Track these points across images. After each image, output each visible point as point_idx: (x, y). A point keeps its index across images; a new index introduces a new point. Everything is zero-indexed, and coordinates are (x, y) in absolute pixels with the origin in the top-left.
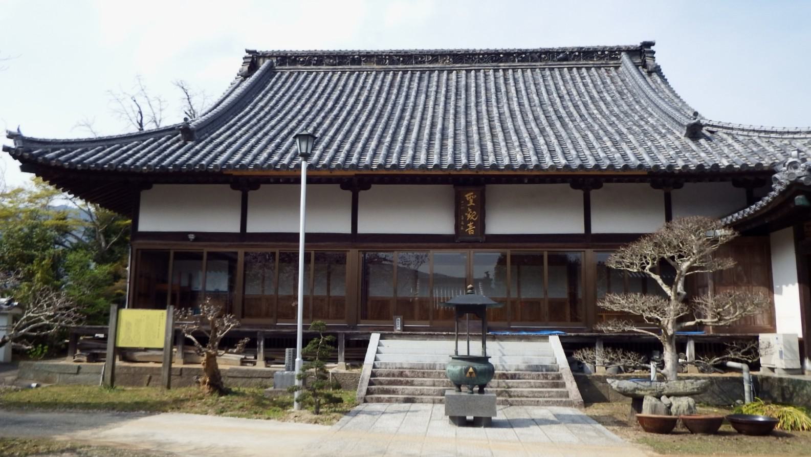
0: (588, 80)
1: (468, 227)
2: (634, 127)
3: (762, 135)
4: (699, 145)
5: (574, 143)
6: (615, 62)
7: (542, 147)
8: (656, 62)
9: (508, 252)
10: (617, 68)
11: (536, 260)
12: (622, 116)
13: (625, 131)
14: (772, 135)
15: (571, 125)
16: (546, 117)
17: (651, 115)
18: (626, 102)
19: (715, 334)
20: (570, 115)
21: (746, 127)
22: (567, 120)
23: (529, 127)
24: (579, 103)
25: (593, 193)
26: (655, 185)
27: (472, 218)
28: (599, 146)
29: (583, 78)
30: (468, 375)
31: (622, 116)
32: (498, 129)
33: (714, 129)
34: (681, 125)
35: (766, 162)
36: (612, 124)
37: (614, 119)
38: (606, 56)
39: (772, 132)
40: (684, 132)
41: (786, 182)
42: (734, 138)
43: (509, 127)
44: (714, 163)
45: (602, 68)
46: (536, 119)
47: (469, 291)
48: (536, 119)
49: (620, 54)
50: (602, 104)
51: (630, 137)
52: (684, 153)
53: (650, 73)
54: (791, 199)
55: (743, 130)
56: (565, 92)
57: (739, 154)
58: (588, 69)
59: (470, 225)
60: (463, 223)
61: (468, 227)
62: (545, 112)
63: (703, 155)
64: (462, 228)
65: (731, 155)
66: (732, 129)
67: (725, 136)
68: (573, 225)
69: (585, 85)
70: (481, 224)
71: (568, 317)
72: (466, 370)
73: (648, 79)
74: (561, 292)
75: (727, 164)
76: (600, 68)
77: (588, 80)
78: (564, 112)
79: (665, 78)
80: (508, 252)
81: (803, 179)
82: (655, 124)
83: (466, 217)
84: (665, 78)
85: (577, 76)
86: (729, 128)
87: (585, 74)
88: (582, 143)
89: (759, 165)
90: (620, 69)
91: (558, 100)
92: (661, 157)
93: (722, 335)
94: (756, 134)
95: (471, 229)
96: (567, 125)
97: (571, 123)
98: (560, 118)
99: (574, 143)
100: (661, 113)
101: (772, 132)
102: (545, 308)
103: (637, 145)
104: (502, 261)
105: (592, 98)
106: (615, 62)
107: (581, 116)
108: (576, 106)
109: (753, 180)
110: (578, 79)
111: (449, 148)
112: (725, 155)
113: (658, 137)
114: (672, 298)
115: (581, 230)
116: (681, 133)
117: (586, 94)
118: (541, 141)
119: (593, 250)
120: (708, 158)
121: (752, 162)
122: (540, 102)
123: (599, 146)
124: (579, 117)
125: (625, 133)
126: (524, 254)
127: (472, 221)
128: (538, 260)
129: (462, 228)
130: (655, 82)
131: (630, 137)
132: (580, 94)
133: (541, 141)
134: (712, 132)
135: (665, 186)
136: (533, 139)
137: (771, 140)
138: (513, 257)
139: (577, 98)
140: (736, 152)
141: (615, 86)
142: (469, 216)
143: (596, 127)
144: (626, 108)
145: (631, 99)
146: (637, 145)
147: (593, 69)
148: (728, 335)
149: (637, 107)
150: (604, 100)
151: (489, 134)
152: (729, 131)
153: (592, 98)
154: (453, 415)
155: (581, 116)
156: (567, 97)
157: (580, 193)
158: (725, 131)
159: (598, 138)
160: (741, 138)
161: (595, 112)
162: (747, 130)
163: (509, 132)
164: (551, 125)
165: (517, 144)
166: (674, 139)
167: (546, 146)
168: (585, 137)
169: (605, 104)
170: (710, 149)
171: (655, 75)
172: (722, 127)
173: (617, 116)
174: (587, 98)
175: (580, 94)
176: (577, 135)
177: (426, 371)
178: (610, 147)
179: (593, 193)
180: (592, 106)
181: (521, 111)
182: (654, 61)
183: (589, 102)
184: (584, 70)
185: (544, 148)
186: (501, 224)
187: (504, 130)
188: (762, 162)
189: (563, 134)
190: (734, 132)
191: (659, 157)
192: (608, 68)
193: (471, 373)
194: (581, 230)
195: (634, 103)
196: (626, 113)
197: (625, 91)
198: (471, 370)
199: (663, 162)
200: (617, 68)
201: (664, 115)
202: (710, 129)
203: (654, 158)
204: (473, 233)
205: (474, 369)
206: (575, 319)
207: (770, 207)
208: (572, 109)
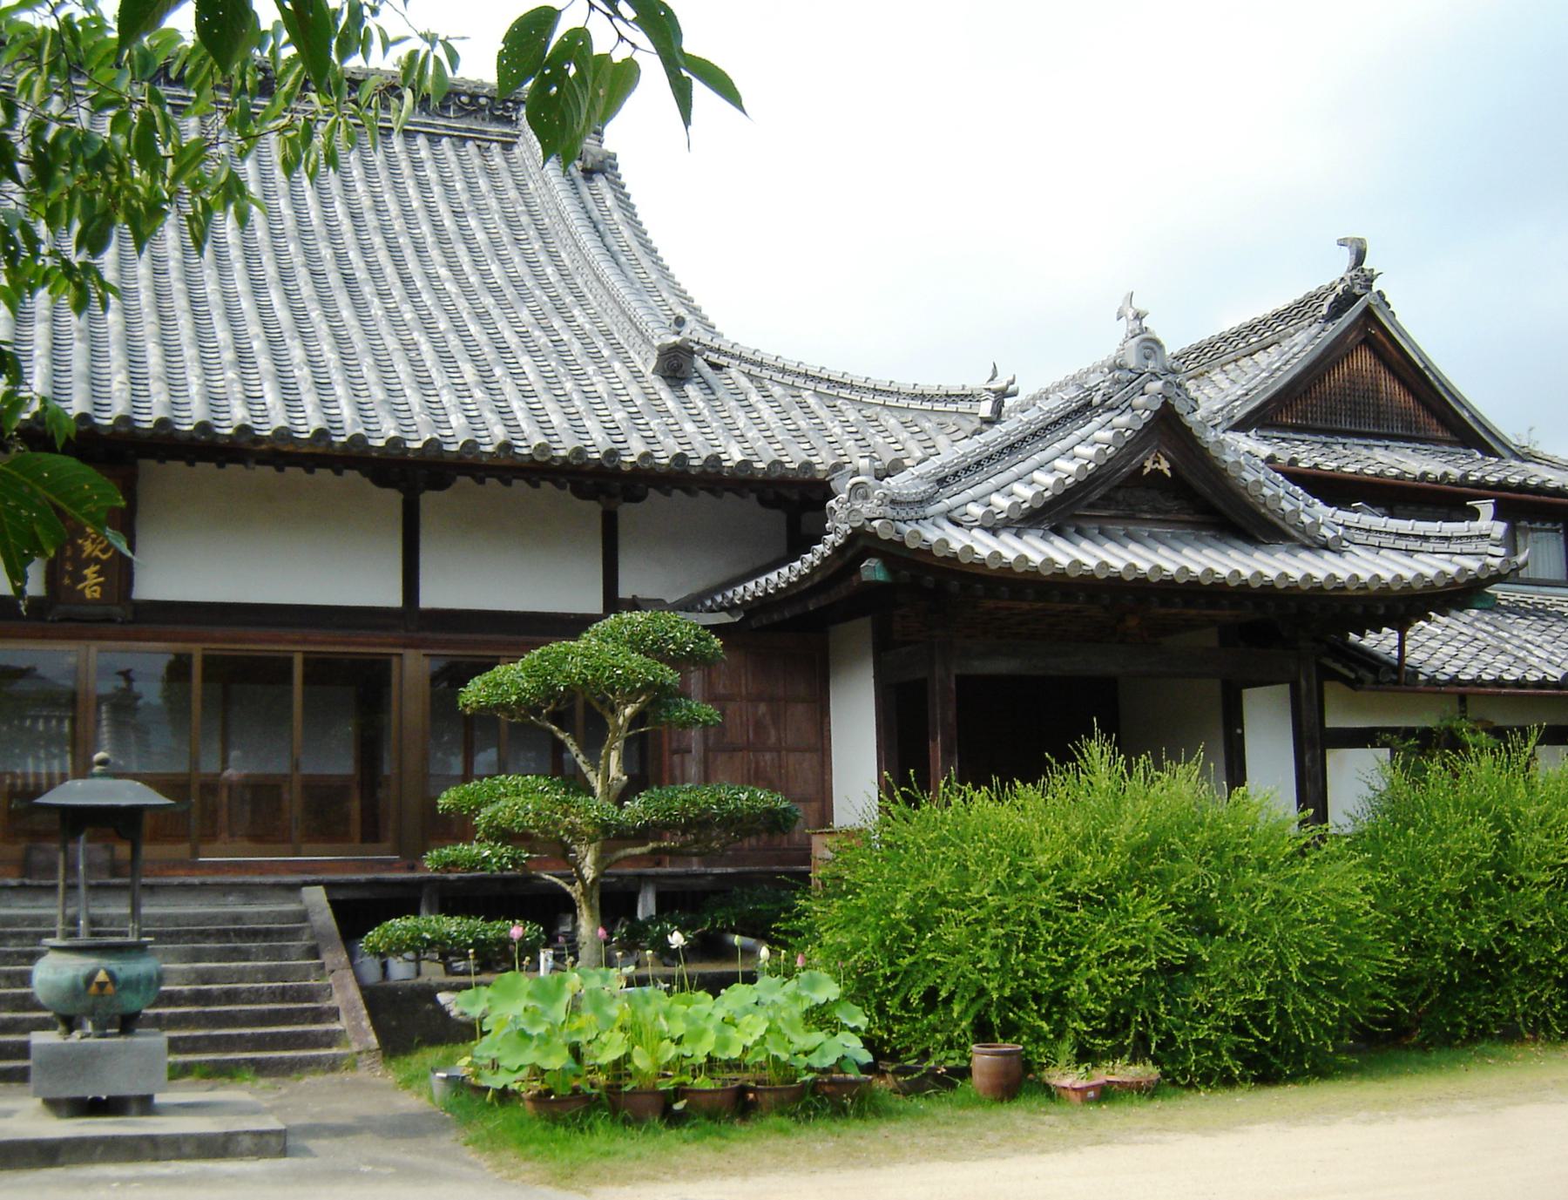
0: (430, 173)
1: (84, 578)
2: (537, 333)
3: (822, 388)
4: (684, 399)
5: (383, 368)
6: (507, 130)
7: (297, 373)
8: (605, 146)
9: (197, 651)
10: (507, 146)
11: (275, 671)
12: (510, 293)
13: (513, 341)
14: (844, 393)
15: (376, 309)
16: (313, 273)
17: (580, 297)
18: (523, 253)
19: (703, 869)
20: (374, 271)
21: (791, 366)
22: (368, 290)
23: (263, 300)
24: (403, 240)
25: (428, 499)
26: (581, 492)
27: (97, 553)
28: (447, 381)
29: (416, 165)
30: (93, 988)
31: (510, 293)
32: (180, 303)
33: (723, 361)
34: (647, 341)
35: (823, 460)
36: (481, 316)
37: (488, 301)
38: (481, 108)
39: (843, 385)
40: (653, 363)
41: (845, 528)
42: (761, 388)
43: (210, 298)
44: (711, 451)
45: (470, 144)
46: (285, 276)
47: (97, 769)
48: (285, 276)
49: (517, 110)
50: (461, 250)
51: (525, 360)
52: (647, 418)
53: (588, 174)
54: (853, 567)
55: (783, 371)
56: (366, 202)
57: (768, 433)
58: (434, 139)
59: (89, 572)
60: (69, 568)
61: (84, 578)
62: (310, 255)
63: (689, 427)
64: (67, 581)
65: (749, 435)
66: (761, 364)
67: (744, 382)
68: (370, 584)
69: (422, 185)
70: (121, 572)
71: (355, 829)
72: (90, 979)
73: (584, 189)
74: (336, 761)
75: (738, 457)
76: (464, 140)
77: (430, 173)
78: (362, 265)
79: (627, 190)
80: (197, 651)
81: (876, 523)
82: (587, 326)
83: (81, 549)
84: (627, 190)
85: (402, 156)
86: (754, 363)
87: (424, 154)
88: (402, 369)
89: (807, 466)
90: (516, 150)
91: (346, 226)
92: (591, 424)
93: (717, 870)
94: (811, 385)
95: (91, 585)
96: (366, 305)
97: (376, 301)
98: (348, 280)
99: (383, 368)
100: (605, 298)
101: (843, 385)
102: (293, 800)
103: (539, 386)
104: (178, 671)
105: (437, 228)
106: (507, 130)
107: (406, 281)
108: (393, 249)
109: (795, 499)
110: (405, 166)
111: (37, 353)
112: (737, 433)
113: (591, 369)
114: (598, 790)
115: (395, 599)
116: (647, 364)
117: (421, 215)
118: (296, 353)
119: (423, 651)
120: (701, 438)
121: (794, 457)
122: (299, 223)
123: (447, 381)
124: (399, 284)
125: (513, 347)
126: (240, 661)
127: (97, 560)
128: (277, 670)
129: (67, 581)
130: (598, 201)
131: (525, 360)
132: (406, 213)
133: (296, 353)
134: (716, 367)
135: (604, 495)
136: (274, 344)
137: (839, 402)
138: (209, 661)
139: (398, 225)
140: (763, 427)
141: (500, 200)
142: (88, 547)
143: (443, 325)
144: (522, 269)
145: (537, 246)
146: (539, 386)
147: (445, 140)
148: (730, 870)
149: (549, 270)
150: (468, 240)
151: (154, 318)
152: (755, 371)
153: (437, 228)
154: (50, 1096)
155: (406, 281)
156: (370, 218)
157: (394, 498)
158: (746, 367)
159: (445, 358)
160: (777, 391)
161: (444, 272)
162: (791, 373)
163: (208, 313)
164: (325, 301)
165: (228, 356)
166: (628, 378)
167: (306, 370)
168: (408, 347)
169: (470, 250)
170: (706, 412)
171: (600, 182)
172: (740, 358)
173: (494, 291)
174: (426, 229)
175: (406, 213)
176: (391, 342)
177: (1529, 750)
178: (471, 386)
179: (428, 499)
180: (434, 253)
181: (245, 248)
182: (601, 142)
183: (430, 240)
184: (421, 141)
185: (302, 374)
186: (173, 572)
187: (195, 303)
188: (814, 459)
189: (356, 334)
190: (766, 374)
191: (588, 423)
192: (486, 144)
193: (102, 985)
194: (395, 599)
195: (543, 258)
196: (516, 283)
197: (525, 219)
198: (102, 976)
199: (598, 442)
200: (507, 146)
201: (610, 305)
202: (714, 358)
203: (580, 430)
204: (97, 595)
205: (110, 974)
206: (372, 833)
207: (817, 578)
208: (383, 256)
